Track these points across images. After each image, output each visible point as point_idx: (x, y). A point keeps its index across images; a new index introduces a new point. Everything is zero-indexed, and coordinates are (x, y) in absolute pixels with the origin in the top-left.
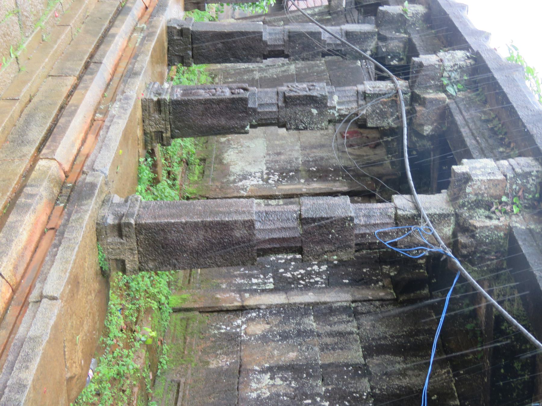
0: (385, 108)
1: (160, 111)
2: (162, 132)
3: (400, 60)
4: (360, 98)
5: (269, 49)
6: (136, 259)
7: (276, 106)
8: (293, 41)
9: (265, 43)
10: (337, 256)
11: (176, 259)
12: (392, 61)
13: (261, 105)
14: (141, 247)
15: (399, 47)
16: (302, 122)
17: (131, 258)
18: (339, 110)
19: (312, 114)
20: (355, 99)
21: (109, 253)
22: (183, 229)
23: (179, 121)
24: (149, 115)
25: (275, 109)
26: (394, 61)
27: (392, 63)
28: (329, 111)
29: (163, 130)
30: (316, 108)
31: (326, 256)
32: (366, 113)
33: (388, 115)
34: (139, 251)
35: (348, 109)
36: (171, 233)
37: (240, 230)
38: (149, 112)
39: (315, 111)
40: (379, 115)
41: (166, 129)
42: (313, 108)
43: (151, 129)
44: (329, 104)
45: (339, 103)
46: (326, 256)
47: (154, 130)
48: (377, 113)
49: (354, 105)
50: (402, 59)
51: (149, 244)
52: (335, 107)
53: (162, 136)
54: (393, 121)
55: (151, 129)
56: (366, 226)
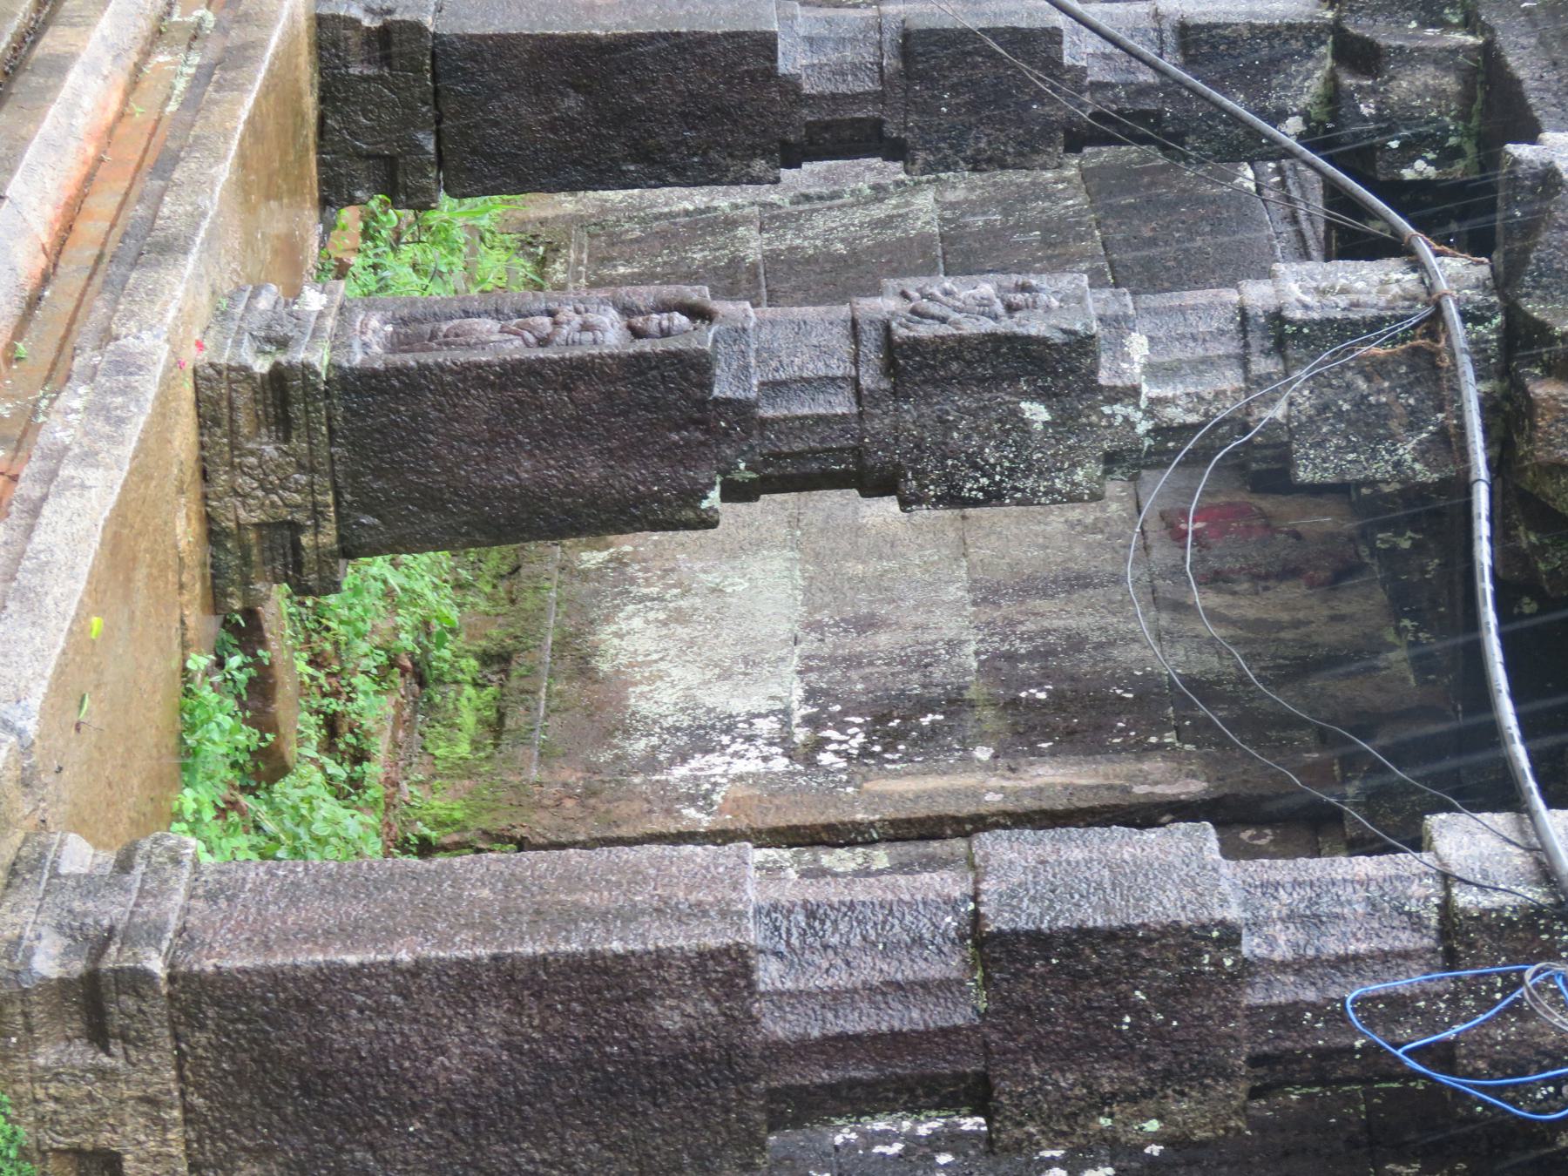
0: (1380, 391)
1: (283, 425)
2: (296, 528)
3: (1447, 157)
4: (1255, 339)
5: (807, 115)
6: (177, 1150)
7: (848, 392)
8: (923, 77)
9: (790, 86)
10: (1160, 1117)
11: (371, 1147)
12: (1409, 162)
13: (774, 388)
14: (199, 1087)
15: (1439, 94)
16: (976, 467)
17: (152, 1145)
18: (1153, 401)
19: (1024, 425)
20: (1234, 347)
21: (41, 1120)
22: (405, 994)
23: (378, 473)
24: (233, 446)
25: (841, 405)
26: (1420, 165)
27: (1408, 174)
28: (1107, 410)
29: (299, 517)
30: (1044, 395)
31: (1105, 1122)
32: (1288, 417)
33: (1393, 424)
34: (187, 1109)
35: (1201, 399)
36: (343, 1018)
37: (682, 997)
38: (233, 432)
39: (1037, 413)
40: (1350, 423)
41: (316, 513)
42: (1027, 396)
43: (242, 514)
44: (1104, 378)
45: (1154, 371)
46: (1105, 1122)
47: (257, 516)
48: (1340, 415)
49: (1230, 380)
50: (1457, 152)
51: (238, 1074)
52: (1134, 392)
53: (297, 547)
54: (1421, 454)
55: (242, 514)
56: (1299, 966)
